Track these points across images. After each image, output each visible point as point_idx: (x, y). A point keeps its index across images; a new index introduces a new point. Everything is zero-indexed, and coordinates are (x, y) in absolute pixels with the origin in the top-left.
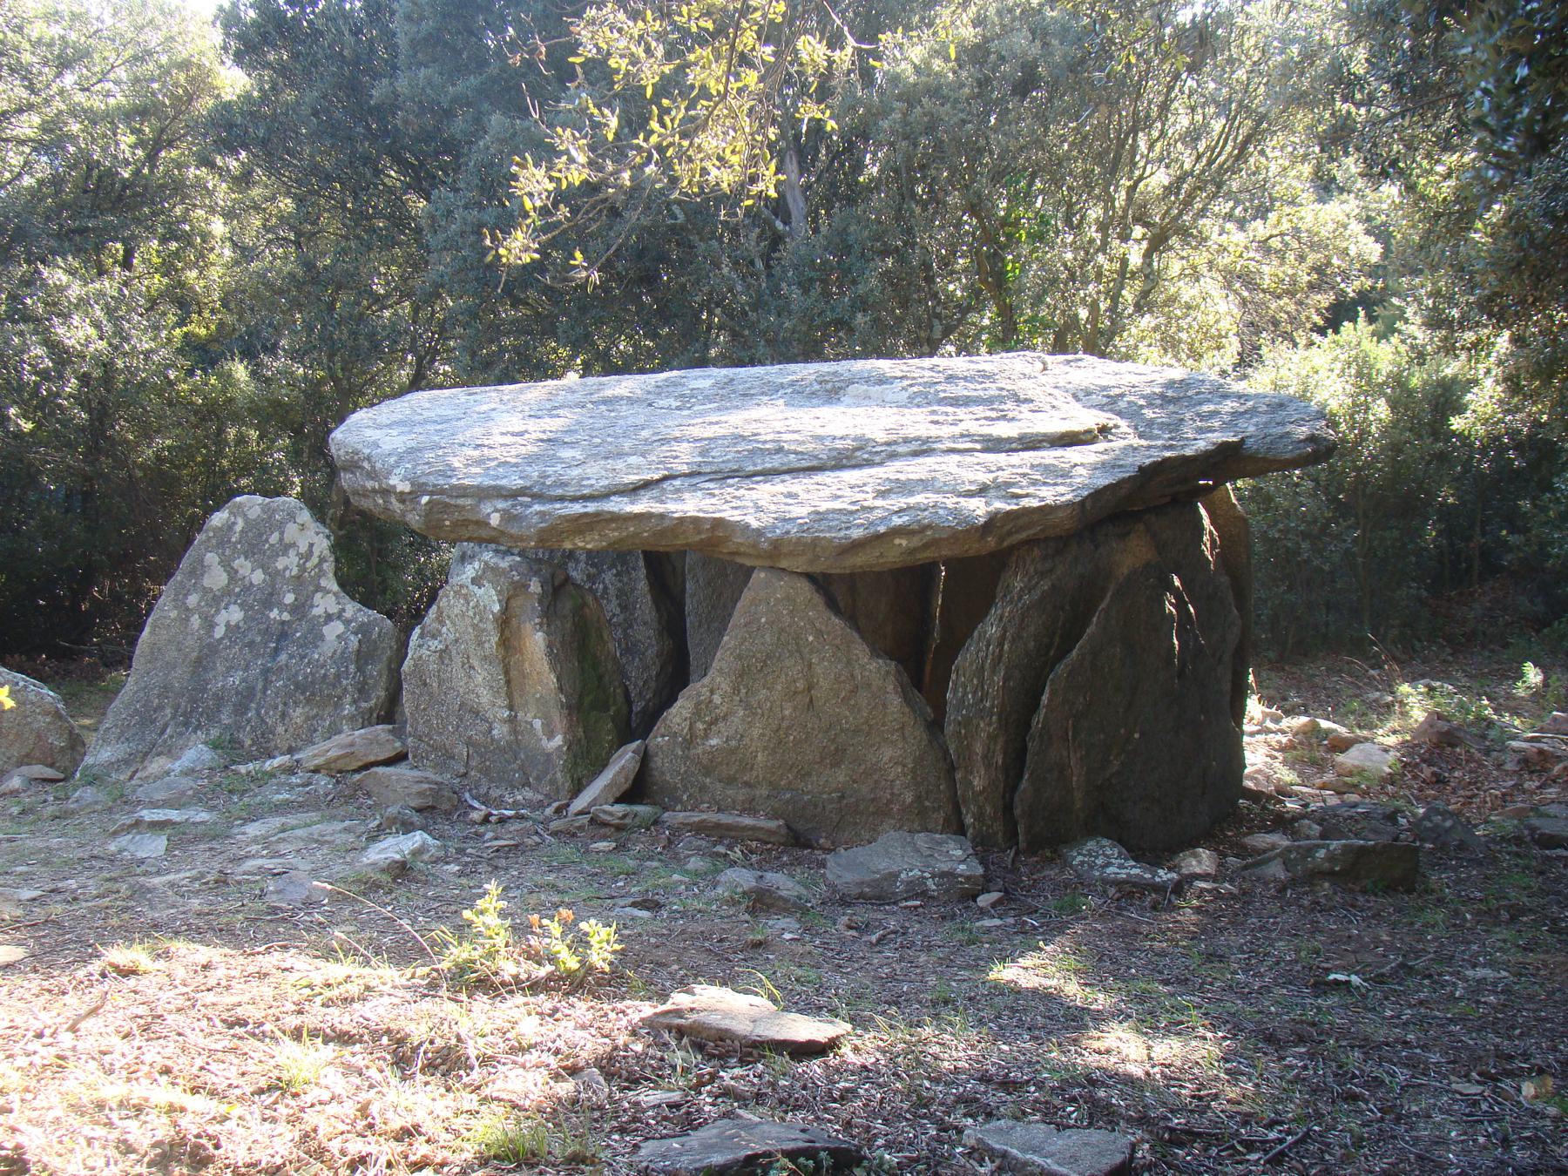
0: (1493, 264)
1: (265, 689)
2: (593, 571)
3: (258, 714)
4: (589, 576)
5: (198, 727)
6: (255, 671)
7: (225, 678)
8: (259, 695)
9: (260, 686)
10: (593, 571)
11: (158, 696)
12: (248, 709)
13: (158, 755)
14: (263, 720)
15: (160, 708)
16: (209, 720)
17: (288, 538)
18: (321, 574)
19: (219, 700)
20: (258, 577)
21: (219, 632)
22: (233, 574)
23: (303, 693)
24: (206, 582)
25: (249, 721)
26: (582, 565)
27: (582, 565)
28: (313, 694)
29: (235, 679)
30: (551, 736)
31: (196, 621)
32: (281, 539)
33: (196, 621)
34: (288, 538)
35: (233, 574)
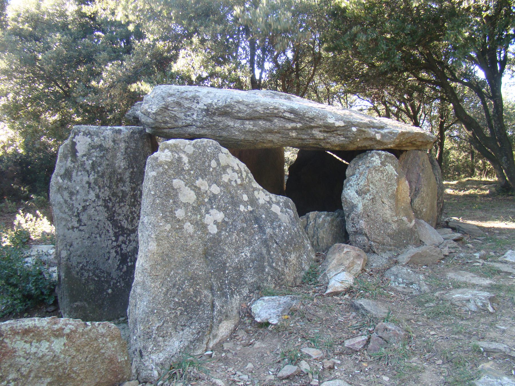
0: (281, 75)
1: (268, 252)
2: (134, 185)
3: (272, 267)
4: (131, 188)
5: (232, 294)
6: (257, 244)
7: (238, 255)
8: (266, 257)
9: (264, 251)
10: (134, 185)
11: (191, 286)
12: (264, 267)
13: (220, 321)
14: (276, 269)
15: (197, 293)
16: (236, 284)
17: (223, 162)
18: (250, 182)
19: (240, 270)
20: (215, 189)
21: (213, 229)
22: (197, 190)
23: (291, 246)
24: (183, 199)
25: (268, 274)
26: (128, 183)
27: (128, 183)
28: (295, 244)
29: (246, 253)
30: (410, 221)
31: (189, 227)
32: (219, 164)
33: (189, 227)
34: (223, 162)
35: (197, 190)
